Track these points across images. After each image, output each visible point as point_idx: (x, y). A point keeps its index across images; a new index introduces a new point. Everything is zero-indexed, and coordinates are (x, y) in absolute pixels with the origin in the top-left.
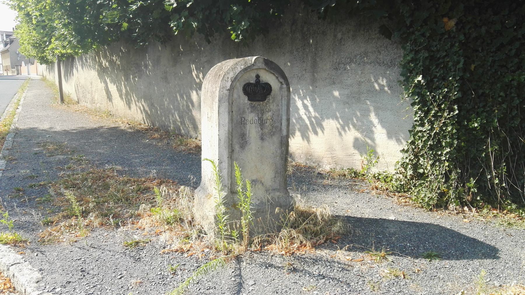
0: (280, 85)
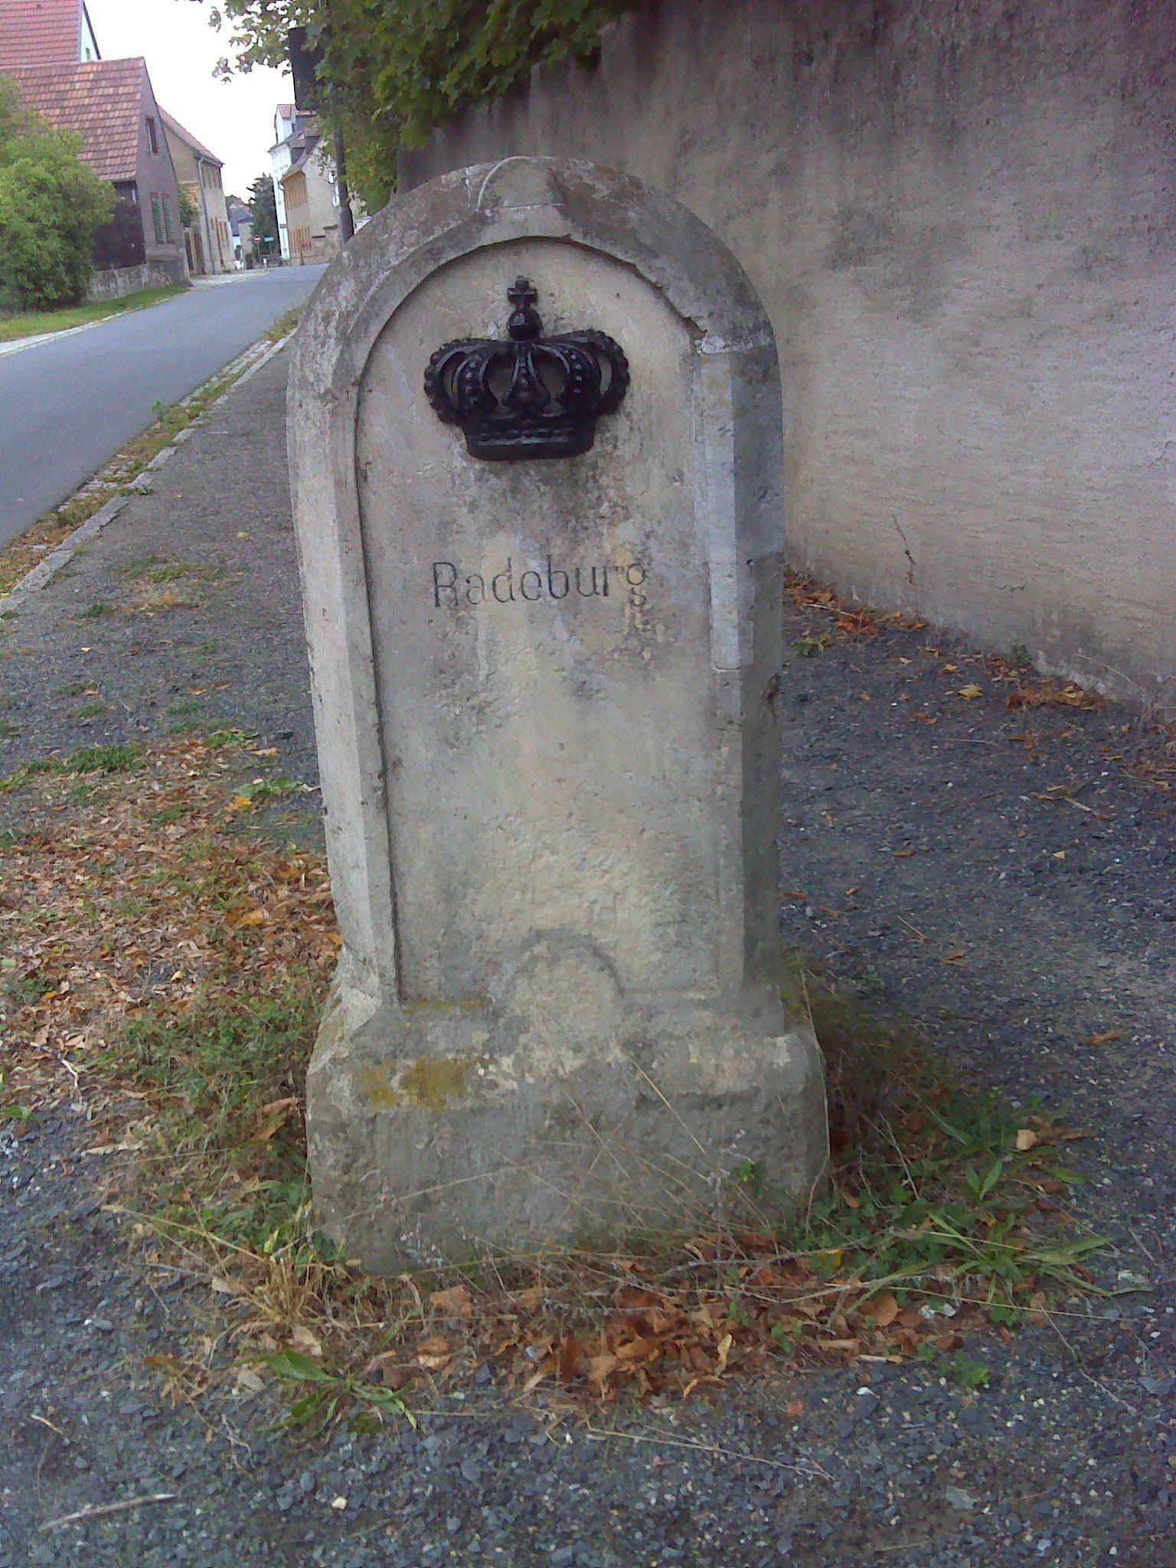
0: (684, 340)
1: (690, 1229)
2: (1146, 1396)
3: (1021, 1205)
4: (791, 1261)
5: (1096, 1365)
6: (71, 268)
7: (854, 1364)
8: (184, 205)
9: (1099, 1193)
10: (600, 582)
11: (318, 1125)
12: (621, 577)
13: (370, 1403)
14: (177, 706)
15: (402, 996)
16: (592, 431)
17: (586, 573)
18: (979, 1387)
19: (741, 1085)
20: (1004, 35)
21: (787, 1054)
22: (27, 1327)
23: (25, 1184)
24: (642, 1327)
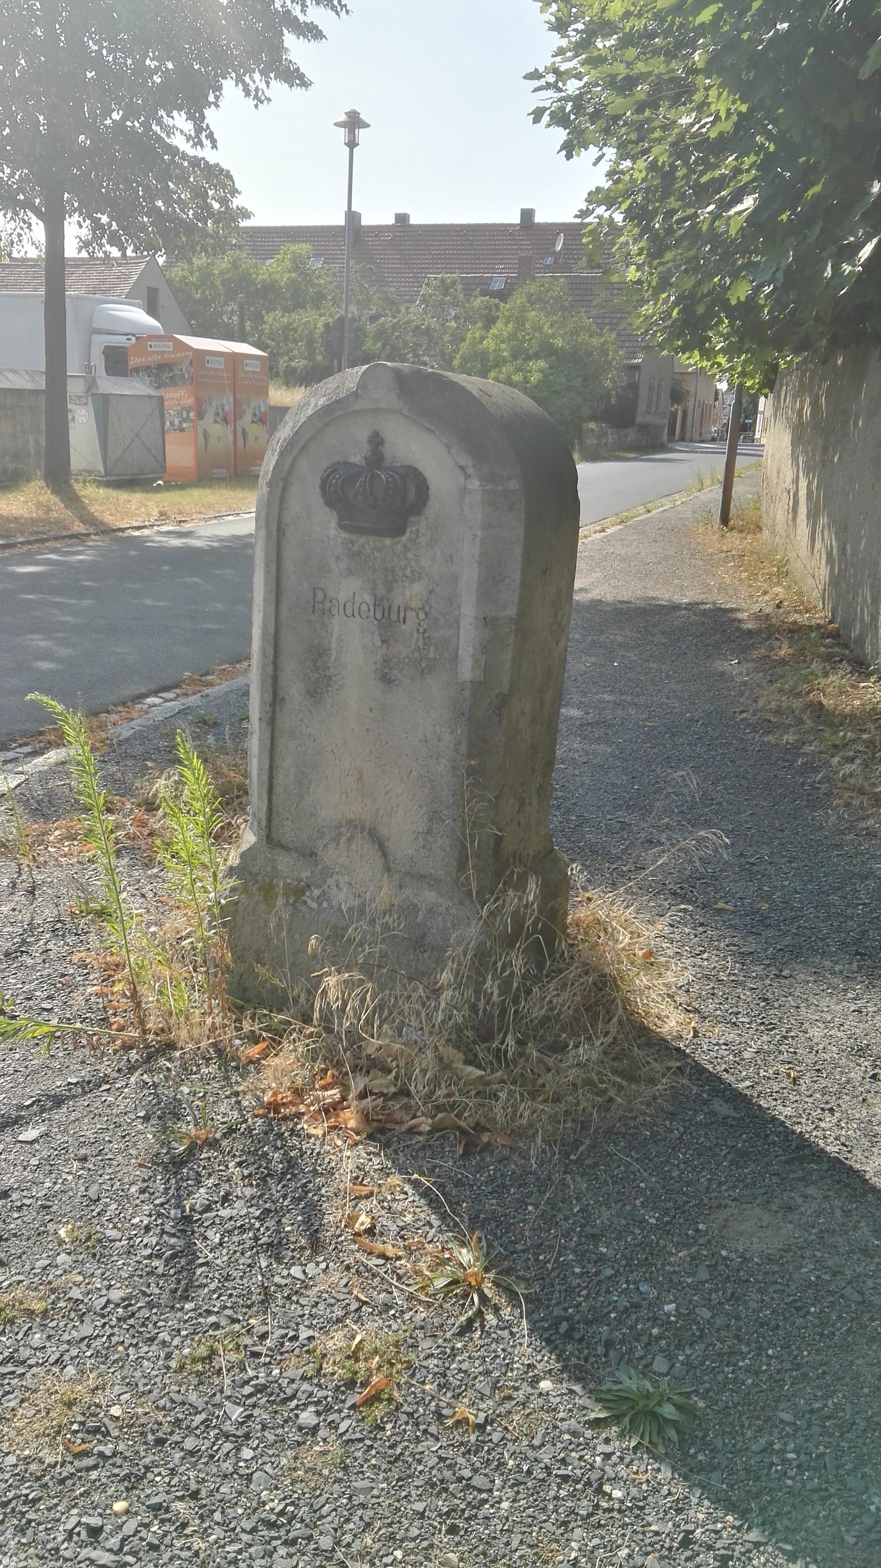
0: (462, 478)
17: (395, 608)
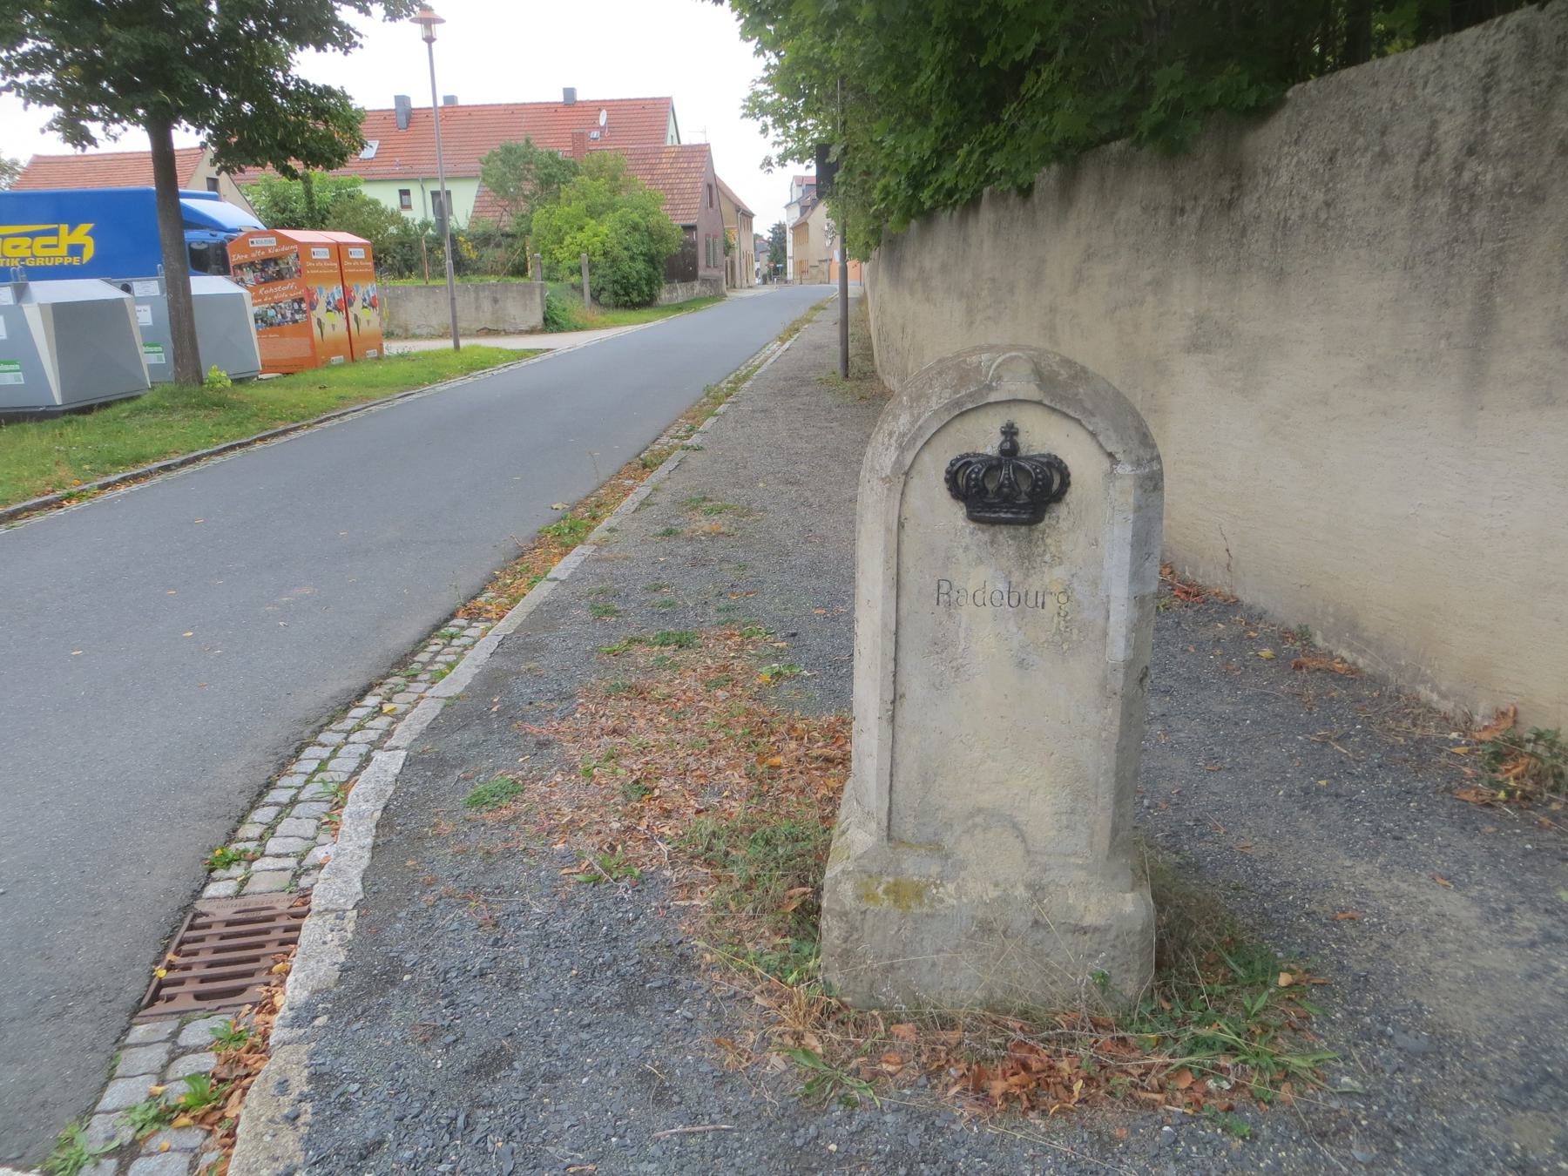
1: (1058, 1008)
2: (1355, 1162)
3: (1278, 1023)
4: (1123, 1039)
5: (1322, 1135)
6: (650, 282)
7: (1161, 1110)
8: (726, 242)
9: (1333, 1023)
10: (1040, 601)
11: (829, 911)
12: (1054, 598)
13: (852, 1088)
14: (722, 606)
15: (889, 838)
16: (1044, 511)
17: (1032, 595)
18: (1243, 1138)
19: (1100, 922)
20: (1323, 216)
21: (1131, 906)
22: (641, 1009)
23: (637, 918)
24: (1025, 1067)
